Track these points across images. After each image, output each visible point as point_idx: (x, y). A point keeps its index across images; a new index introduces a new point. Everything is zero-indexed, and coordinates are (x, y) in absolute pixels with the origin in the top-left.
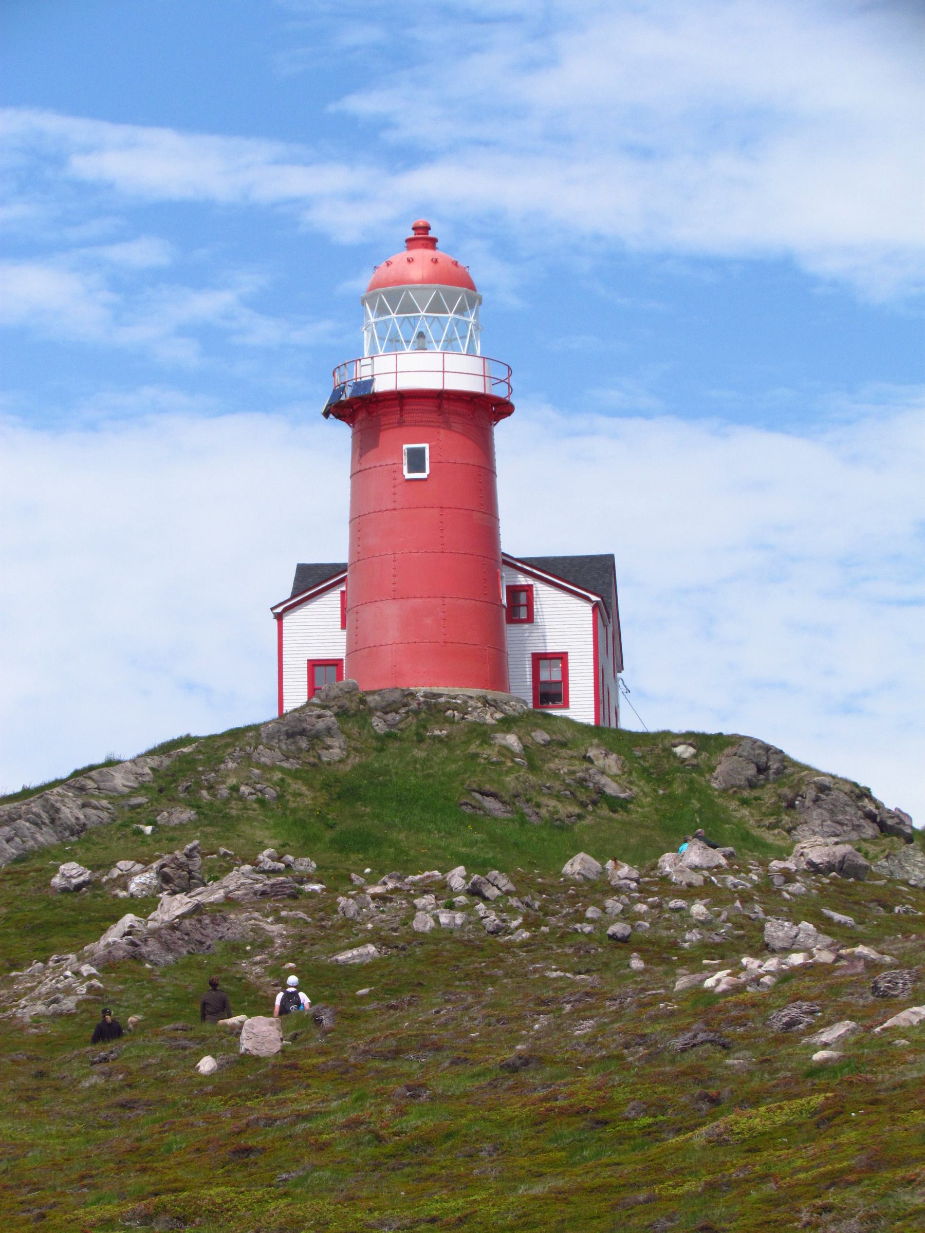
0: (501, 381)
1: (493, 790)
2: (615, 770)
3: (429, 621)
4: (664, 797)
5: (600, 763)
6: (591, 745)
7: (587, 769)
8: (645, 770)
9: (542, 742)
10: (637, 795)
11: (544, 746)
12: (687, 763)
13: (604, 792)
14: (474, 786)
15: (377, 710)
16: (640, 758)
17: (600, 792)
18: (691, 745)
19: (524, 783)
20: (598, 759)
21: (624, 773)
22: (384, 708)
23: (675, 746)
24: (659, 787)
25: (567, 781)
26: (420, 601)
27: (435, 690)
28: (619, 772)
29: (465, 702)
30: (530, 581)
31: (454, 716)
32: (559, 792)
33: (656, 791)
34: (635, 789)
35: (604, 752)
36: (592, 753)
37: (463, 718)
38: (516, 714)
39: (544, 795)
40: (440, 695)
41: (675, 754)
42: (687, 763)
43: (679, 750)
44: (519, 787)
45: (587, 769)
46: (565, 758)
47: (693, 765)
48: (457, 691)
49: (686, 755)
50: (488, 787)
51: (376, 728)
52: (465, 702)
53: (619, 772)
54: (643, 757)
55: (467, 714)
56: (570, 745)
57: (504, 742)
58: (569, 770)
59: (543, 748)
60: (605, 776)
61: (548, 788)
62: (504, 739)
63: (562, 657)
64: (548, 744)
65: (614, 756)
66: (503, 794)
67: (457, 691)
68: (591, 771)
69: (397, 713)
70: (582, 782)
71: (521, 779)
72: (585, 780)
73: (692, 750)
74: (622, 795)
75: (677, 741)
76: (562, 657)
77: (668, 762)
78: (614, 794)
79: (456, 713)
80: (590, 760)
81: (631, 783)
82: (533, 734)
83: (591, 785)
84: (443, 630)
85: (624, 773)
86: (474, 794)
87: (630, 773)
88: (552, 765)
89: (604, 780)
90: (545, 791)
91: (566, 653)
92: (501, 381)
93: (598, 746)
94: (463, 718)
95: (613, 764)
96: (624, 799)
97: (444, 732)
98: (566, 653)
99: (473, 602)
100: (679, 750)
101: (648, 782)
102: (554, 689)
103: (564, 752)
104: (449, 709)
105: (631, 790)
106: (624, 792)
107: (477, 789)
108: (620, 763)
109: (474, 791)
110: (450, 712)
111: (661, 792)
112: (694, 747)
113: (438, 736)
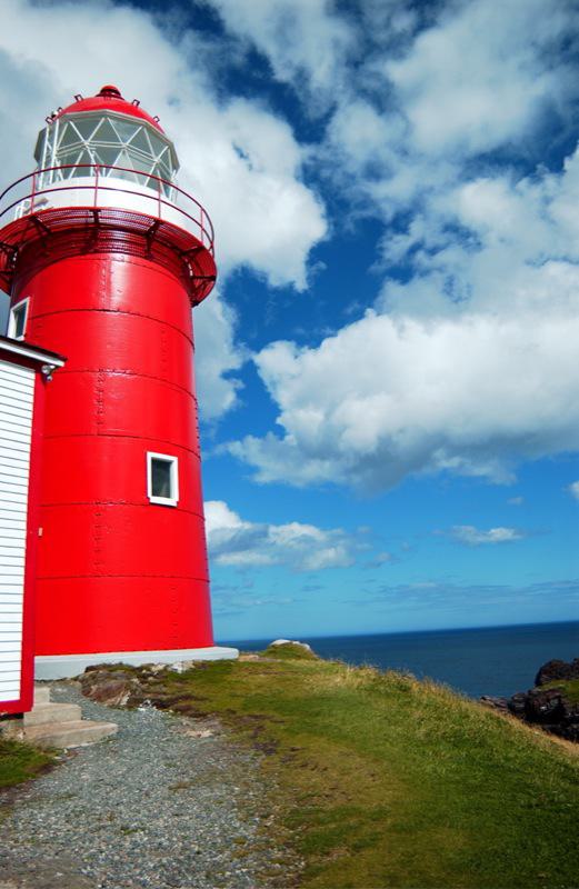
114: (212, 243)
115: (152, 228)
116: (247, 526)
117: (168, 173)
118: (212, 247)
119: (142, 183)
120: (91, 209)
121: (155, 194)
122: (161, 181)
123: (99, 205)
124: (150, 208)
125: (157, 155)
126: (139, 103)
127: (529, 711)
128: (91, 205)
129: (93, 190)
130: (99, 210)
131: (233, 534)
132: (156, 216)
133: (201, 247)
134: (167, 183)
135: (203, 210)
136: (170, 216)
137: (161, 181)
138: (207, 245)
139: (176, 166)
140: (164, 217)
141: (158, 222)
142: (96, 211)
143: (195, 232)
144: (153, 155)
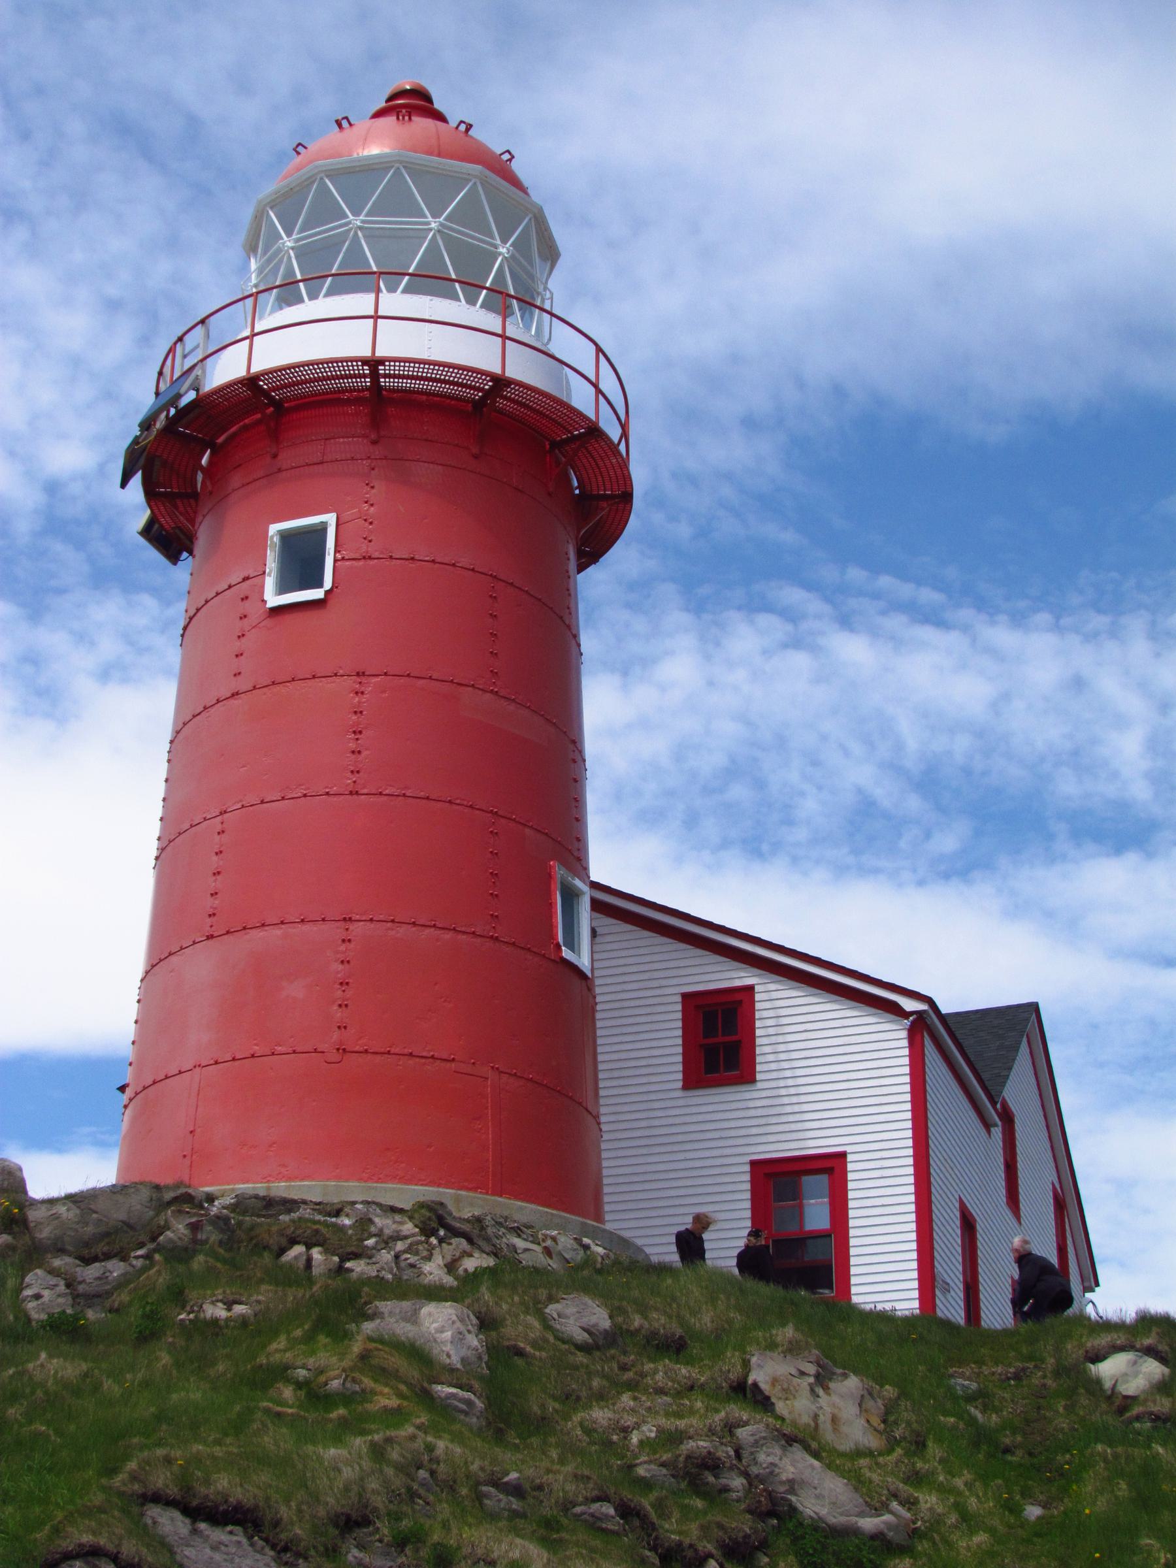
0: (595, 386)
1: (238, 1495)
2: (857, 1432)
3: (296, 990)
4: (1042, 1529)
5: (798, 1407)
6: (772, 1346)
7: (730, 1427)
8: (980, 1437)
9: (581, 1337)
10: (937, 1522)
11: (583, 1348)
12: (1136, 1410)
13: (793, 1510)
14: (161, 1480)
15: (61, 1251)
16: (970, 1398)
17: (775, 1509)
18: (1150, 1352)
19: (408, 1468)
20: (788, 1393)
21: (892, 1444)
22: (87, 1245)
23: (1097, 1358)
24: (1026, 1494)
25: (641, 1471)
26: (277, 932)
27: (280, 1189)
28: (873, 1442)
29: (364, 1223)
30: (742, 977)
31: (309, 1260)
32: (567, 1506)
33: (1013, 1509)
34: (929, 1501)
35: (811, 1369)
36: (765, 1371)
37: (340, 1270)
38: (554, 1264)
39: (493, 1517)
40: (290, 1205)
41: (1098, 1382)
42: (1136, 1410)
43: (1110, 1368)
44: (373, 1484)
45: (730, 1427)
46: (661, 1391)
47: (1157, 1418)
48: (354, 1190)
49: (1131, 1388)
50: (224, 1485)
51: (31, 1305)
52: (364, 1223)
53: (873, 1442)
54: (981, 1397)
55: (356, 1256)
56: (695, 1349)
57: (403, 1330)
58: (660, 1430)
59: (581, 1358)
60: (797, 1452)
61: (517, 1490)
62: (413, 1318)
63: (832, 1166)
64: (599, 1344)
65: (853, 1383)
66: (284, 1512)
67: (354, 1190)
68: (743, 1433)
69: (124, 1259)
70: (698, 1474)
71: (394, 1454)
72: (711, 1464)
73: (1153, 1369)
74: (869, 1524)
75: (1103, 1340)
76: (832, 1166)
77: (1070, 1409)
78: (836, 1519)
79: (316, 1254)
80: (761, 1401)
81: (916, 1479)
82: (552, 1309)
83: (738, 1482)
84: (338, 1014)
85: (892, 1444)
86: (154, 1512)
87: (918, 1445)
88: (600, 1415)
89: (793, 1465)
90: (497, 1500)
91: (843, 1156)
92: (595, 386)
93: (792, 1350)
94: (340, 1270)
95: (849, 1411)
96: (877, 1536)
97: (239, 1309)
98: (843, 1156)
99: (448, 936)
100: (1110, 1368)
101: (984, 1477)
102: (814, 1254)
103: (660, 1371)
104: (293, 1242)
105: (910, 1503)
106: (883, 1508)
107: (173, 1491)
108: (876, 1407)
109: (157, 1498)
110: (298, 1249)
111: (1033, 1512)
112: (1163, 1360)
113: (215, 1321)
114: (624, 427)
115: (487, 394)
116: (736, 1271)
117: (532, 277)
118: (625, 435)
119: (471, 301)
120: (365, 362)
121: (492, 321)
122: (516, 298)
123: (380, 353)
124: (480, 355)
125: (504, 241)
126: (469, 127)
127: (410, 150)
128: (367, 353)
129: (372, 321)
130: (381, 361)
131: (287, 457)
132: (497, 370)
133: (594, 431)
134: (528, 304)
135: (599, 350)
136: (522, 368)
137: (516, 298)
138: (614, 433)
139: (551, 254)
140: (513, 372)
141: (500, 382)
142: (374, 363)
143: (581, 398)
144: (499, 242)
